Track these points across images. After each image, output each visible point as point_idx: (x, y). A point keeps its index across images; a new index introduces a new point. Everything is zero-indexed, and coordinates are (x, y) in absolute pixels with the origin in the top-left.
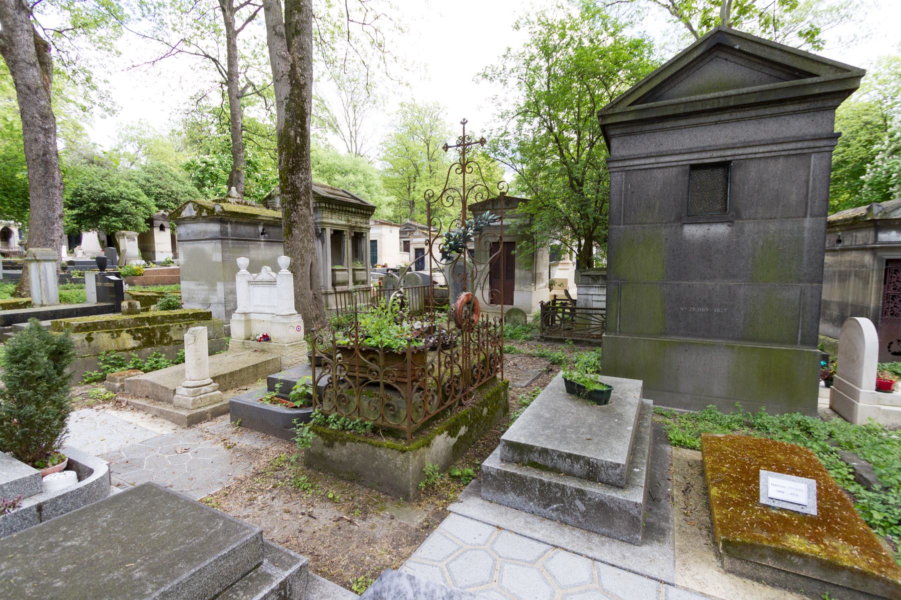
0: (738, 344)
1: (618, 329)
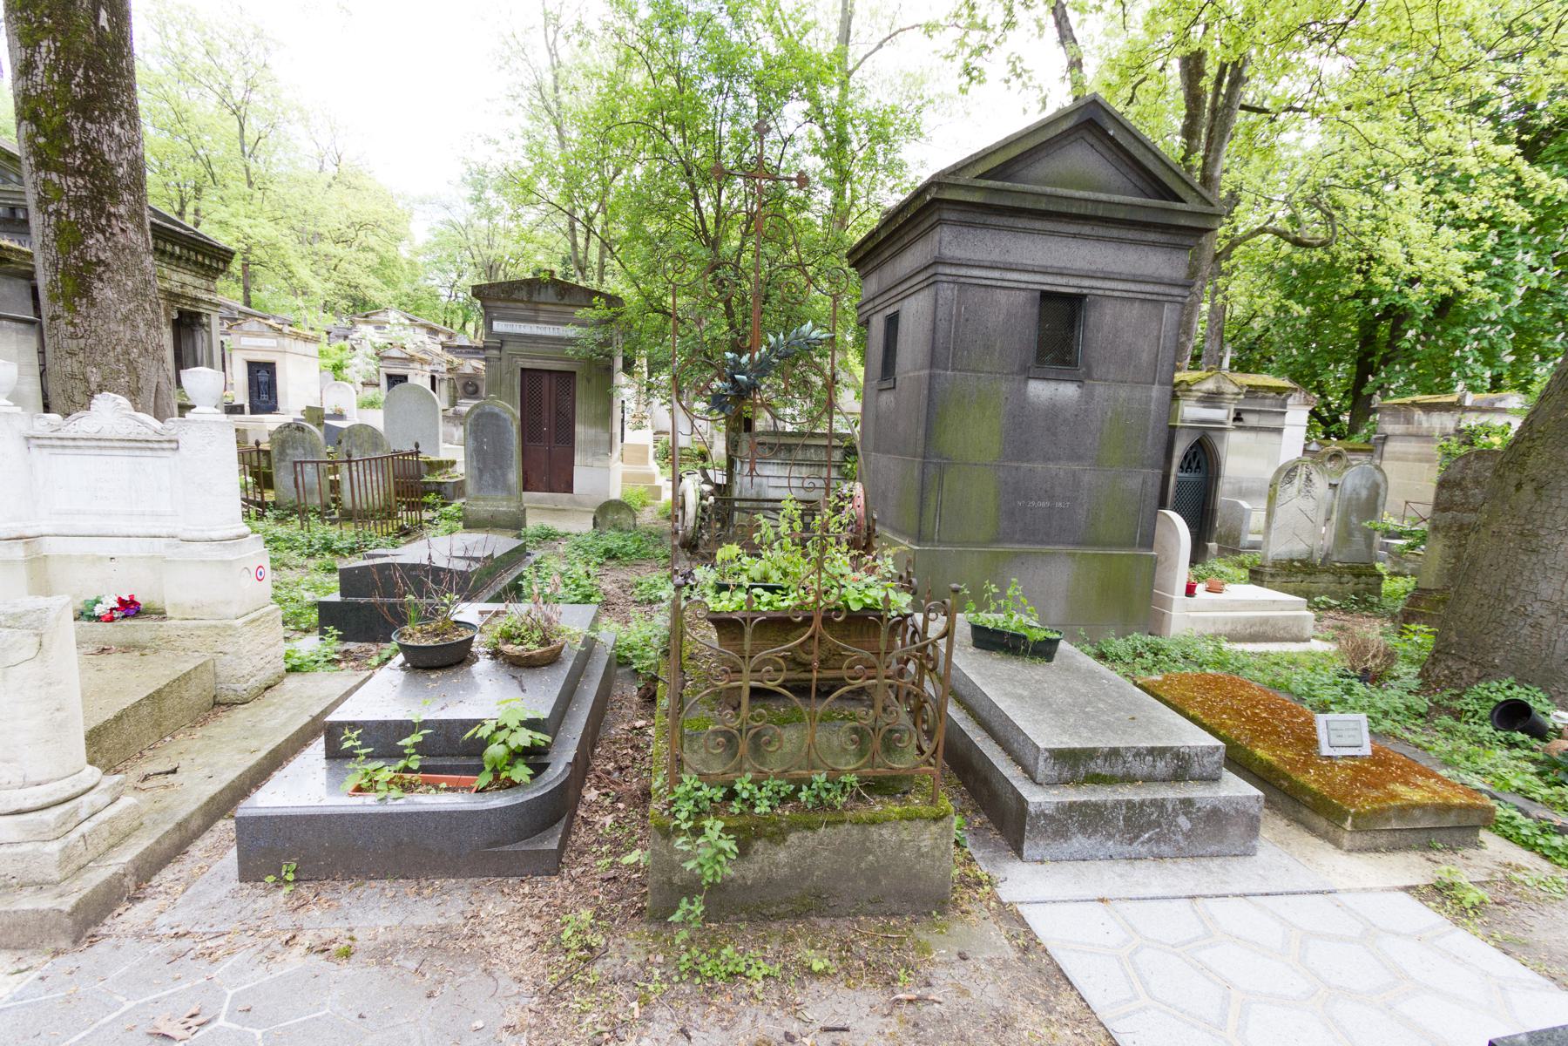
0: (1079, 551)
1: (936, 537)
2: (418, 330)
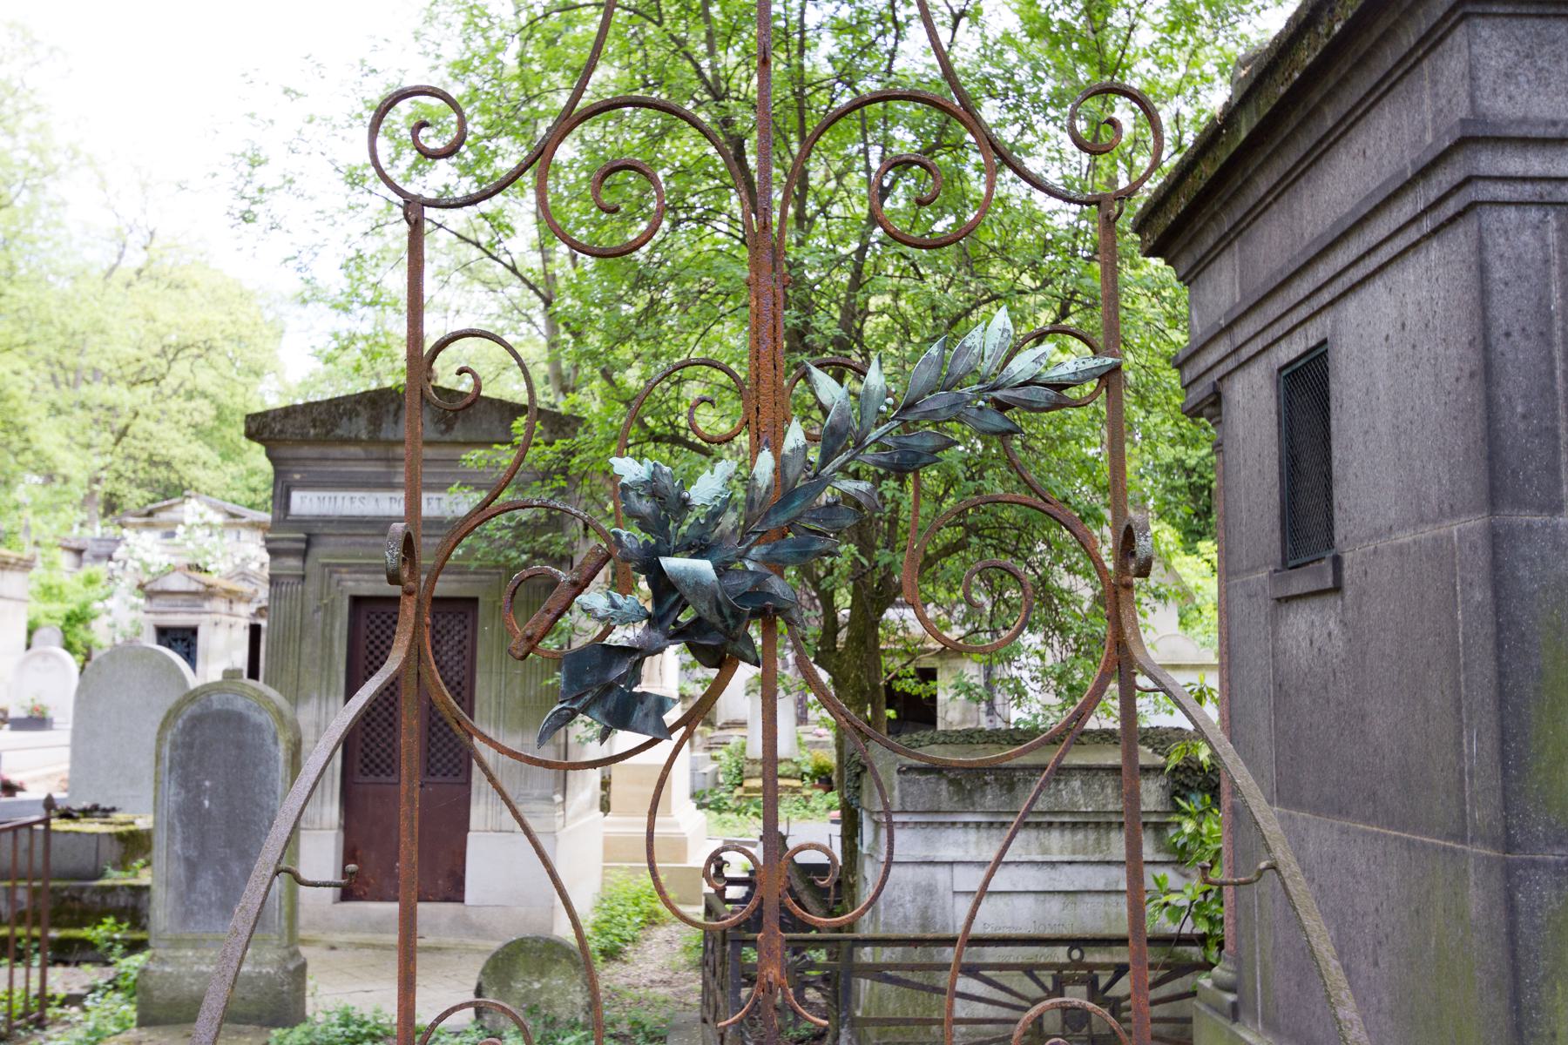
2: (245, 534)
